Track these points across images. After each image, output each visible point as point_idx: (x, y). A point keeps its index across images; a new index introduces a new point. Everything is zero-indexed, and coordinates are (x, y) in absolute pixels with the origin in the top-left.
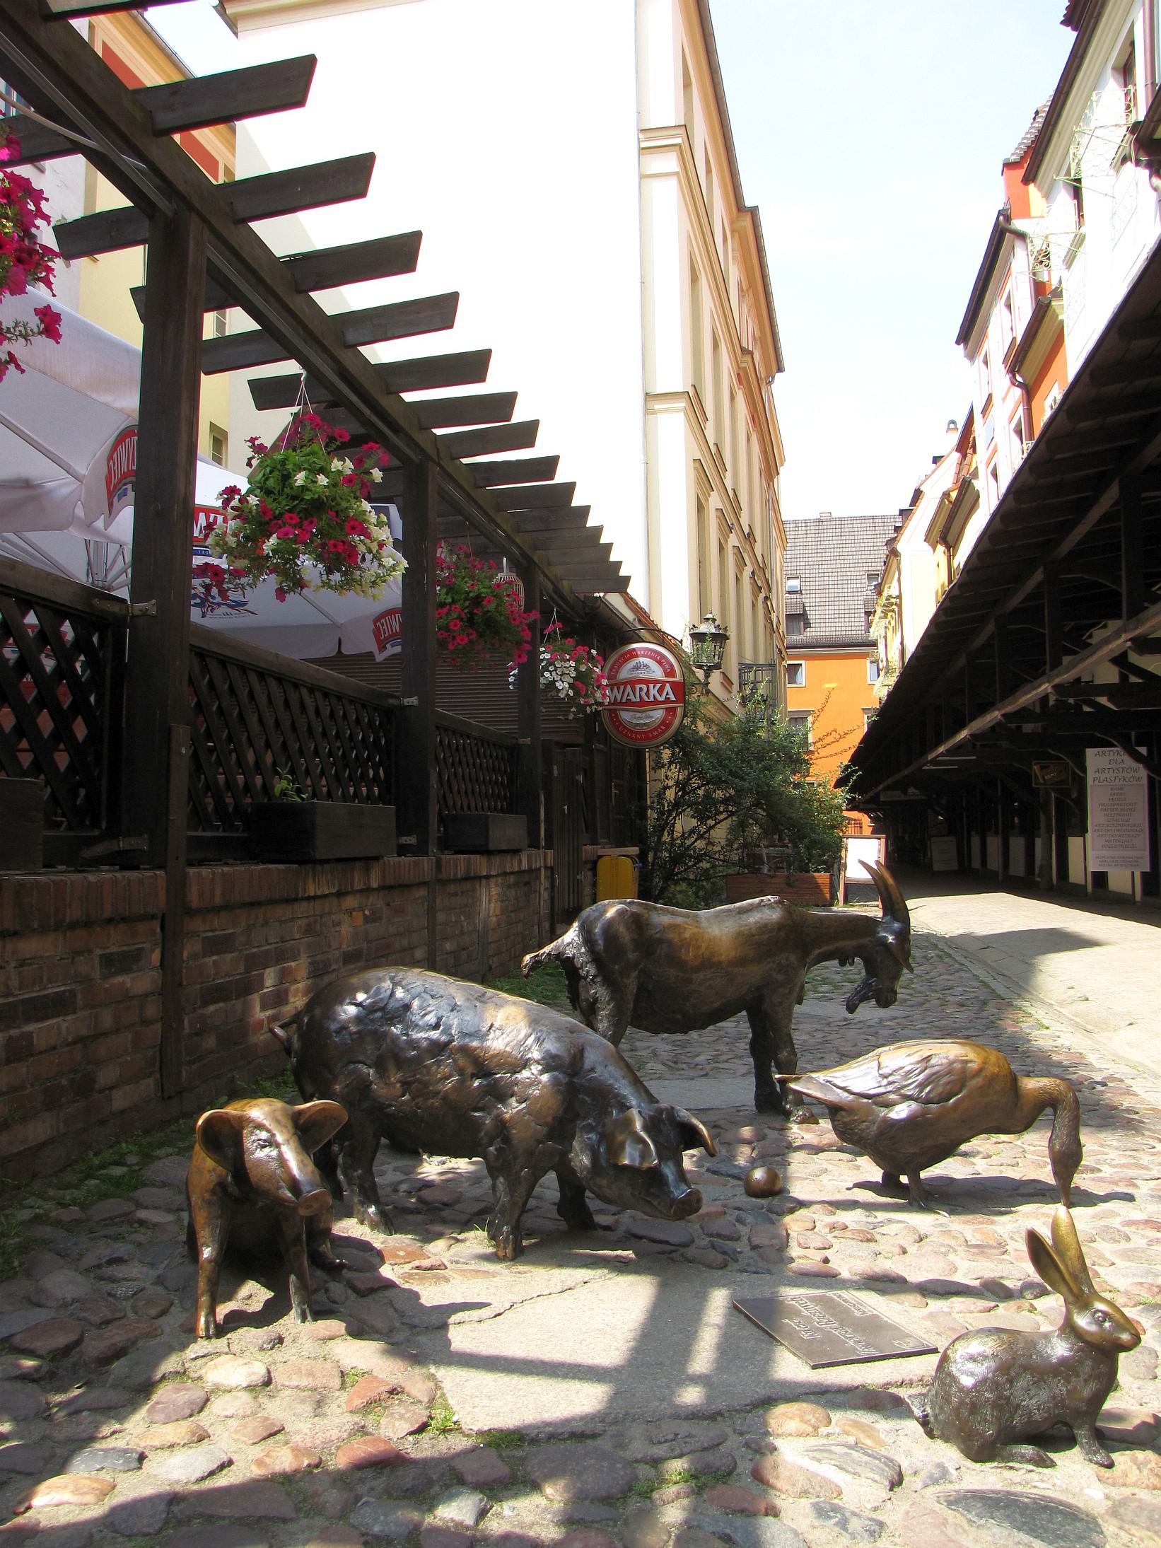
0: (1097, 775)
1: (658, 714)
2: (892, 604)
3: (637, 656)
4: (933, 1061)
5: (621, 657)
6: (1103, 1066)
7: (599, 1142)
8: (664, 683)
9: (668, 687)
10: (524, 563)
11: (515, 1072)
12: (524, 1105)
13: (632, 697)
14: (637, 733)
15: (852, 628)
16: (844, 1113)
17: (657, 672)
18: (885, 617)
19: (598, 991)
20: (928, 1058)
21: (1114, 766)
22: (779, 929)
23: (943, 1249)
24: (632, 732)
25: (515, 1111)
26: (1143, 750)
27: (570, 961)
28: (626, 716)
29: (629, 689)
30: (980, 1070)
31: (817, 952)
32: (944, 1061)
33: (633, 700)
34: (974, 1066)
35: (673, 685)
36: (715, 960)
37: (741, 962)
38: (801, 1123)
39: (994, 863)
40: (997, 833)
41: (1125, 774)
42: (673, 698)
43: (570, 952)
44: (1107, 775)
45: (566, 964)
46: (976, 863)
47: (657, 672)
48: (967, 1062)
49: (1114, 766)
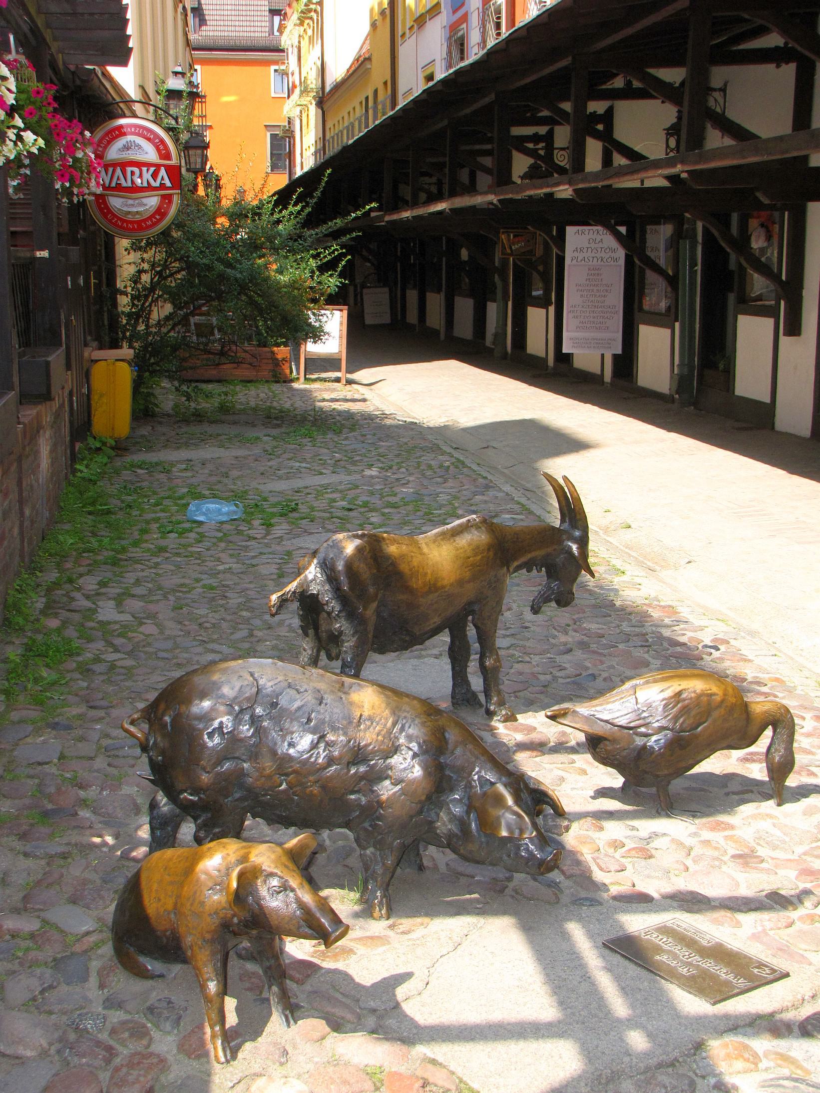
0: (576, 254)
1: (152, 202)
2: (310, 11)
3: (125, 134)
4: (684, 696)
5: (107, 134)
6: (702, 623)
7: (468, 813)
8: (158, 166)
9: (163, 172)
10: (33, 42)
11: (387, 758)
12: (399, 787)
13: (122, 181)
14: (128, 222)
15: (256, 28)
16: (607, 743)
17: (150, 154)
18: (302, 24)
19: (340, 624)
20: (679, 693)
21: (593, 245)
22: (489, 550)
23: (717, 863)
24: (123, 221)
25: (391, 793)
26: (623, 230)
27: (314, 598)
28: (116, 203)
29: (119, 171)
30: (722, 701)
31: (516, 564)
32: (693, 695)
33: (124, 184)
34: (718, 699)
35: (168, 169)
36: (439, 584)
37: (460, 583)
38: (505, 721)
39: (435, 318)
40: (439, 291)
41: (603, 255)
42: (168, 184)
43: (314, 589)
44: (585, 255)
45: (309, 604)
46: (412, 317)
47: (150, 154)
48: (711, 695)
49: (593, 245)
